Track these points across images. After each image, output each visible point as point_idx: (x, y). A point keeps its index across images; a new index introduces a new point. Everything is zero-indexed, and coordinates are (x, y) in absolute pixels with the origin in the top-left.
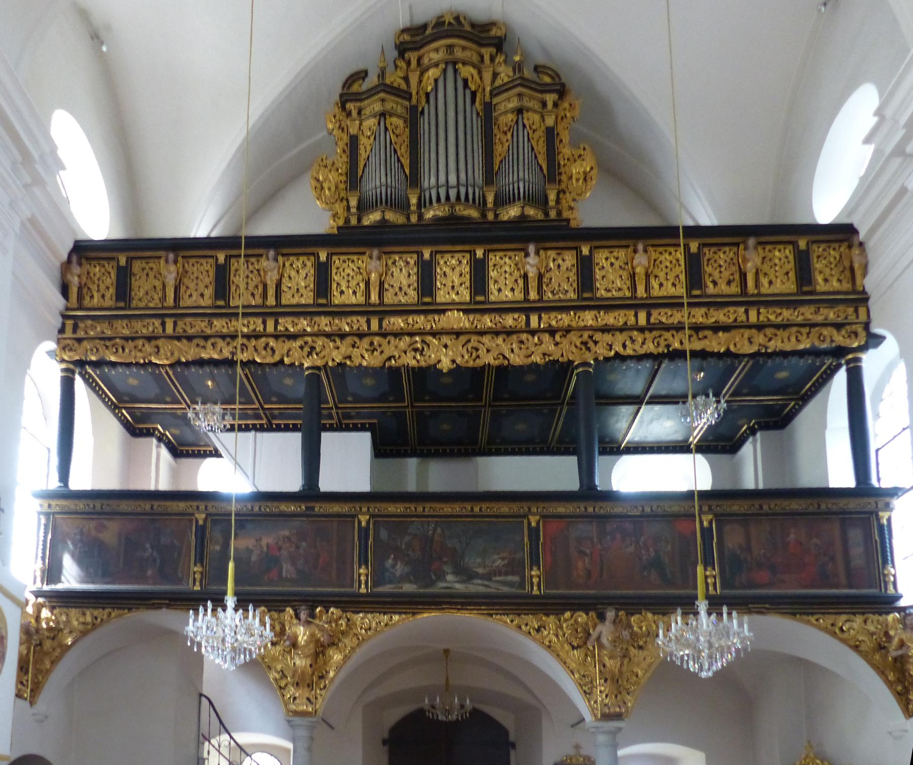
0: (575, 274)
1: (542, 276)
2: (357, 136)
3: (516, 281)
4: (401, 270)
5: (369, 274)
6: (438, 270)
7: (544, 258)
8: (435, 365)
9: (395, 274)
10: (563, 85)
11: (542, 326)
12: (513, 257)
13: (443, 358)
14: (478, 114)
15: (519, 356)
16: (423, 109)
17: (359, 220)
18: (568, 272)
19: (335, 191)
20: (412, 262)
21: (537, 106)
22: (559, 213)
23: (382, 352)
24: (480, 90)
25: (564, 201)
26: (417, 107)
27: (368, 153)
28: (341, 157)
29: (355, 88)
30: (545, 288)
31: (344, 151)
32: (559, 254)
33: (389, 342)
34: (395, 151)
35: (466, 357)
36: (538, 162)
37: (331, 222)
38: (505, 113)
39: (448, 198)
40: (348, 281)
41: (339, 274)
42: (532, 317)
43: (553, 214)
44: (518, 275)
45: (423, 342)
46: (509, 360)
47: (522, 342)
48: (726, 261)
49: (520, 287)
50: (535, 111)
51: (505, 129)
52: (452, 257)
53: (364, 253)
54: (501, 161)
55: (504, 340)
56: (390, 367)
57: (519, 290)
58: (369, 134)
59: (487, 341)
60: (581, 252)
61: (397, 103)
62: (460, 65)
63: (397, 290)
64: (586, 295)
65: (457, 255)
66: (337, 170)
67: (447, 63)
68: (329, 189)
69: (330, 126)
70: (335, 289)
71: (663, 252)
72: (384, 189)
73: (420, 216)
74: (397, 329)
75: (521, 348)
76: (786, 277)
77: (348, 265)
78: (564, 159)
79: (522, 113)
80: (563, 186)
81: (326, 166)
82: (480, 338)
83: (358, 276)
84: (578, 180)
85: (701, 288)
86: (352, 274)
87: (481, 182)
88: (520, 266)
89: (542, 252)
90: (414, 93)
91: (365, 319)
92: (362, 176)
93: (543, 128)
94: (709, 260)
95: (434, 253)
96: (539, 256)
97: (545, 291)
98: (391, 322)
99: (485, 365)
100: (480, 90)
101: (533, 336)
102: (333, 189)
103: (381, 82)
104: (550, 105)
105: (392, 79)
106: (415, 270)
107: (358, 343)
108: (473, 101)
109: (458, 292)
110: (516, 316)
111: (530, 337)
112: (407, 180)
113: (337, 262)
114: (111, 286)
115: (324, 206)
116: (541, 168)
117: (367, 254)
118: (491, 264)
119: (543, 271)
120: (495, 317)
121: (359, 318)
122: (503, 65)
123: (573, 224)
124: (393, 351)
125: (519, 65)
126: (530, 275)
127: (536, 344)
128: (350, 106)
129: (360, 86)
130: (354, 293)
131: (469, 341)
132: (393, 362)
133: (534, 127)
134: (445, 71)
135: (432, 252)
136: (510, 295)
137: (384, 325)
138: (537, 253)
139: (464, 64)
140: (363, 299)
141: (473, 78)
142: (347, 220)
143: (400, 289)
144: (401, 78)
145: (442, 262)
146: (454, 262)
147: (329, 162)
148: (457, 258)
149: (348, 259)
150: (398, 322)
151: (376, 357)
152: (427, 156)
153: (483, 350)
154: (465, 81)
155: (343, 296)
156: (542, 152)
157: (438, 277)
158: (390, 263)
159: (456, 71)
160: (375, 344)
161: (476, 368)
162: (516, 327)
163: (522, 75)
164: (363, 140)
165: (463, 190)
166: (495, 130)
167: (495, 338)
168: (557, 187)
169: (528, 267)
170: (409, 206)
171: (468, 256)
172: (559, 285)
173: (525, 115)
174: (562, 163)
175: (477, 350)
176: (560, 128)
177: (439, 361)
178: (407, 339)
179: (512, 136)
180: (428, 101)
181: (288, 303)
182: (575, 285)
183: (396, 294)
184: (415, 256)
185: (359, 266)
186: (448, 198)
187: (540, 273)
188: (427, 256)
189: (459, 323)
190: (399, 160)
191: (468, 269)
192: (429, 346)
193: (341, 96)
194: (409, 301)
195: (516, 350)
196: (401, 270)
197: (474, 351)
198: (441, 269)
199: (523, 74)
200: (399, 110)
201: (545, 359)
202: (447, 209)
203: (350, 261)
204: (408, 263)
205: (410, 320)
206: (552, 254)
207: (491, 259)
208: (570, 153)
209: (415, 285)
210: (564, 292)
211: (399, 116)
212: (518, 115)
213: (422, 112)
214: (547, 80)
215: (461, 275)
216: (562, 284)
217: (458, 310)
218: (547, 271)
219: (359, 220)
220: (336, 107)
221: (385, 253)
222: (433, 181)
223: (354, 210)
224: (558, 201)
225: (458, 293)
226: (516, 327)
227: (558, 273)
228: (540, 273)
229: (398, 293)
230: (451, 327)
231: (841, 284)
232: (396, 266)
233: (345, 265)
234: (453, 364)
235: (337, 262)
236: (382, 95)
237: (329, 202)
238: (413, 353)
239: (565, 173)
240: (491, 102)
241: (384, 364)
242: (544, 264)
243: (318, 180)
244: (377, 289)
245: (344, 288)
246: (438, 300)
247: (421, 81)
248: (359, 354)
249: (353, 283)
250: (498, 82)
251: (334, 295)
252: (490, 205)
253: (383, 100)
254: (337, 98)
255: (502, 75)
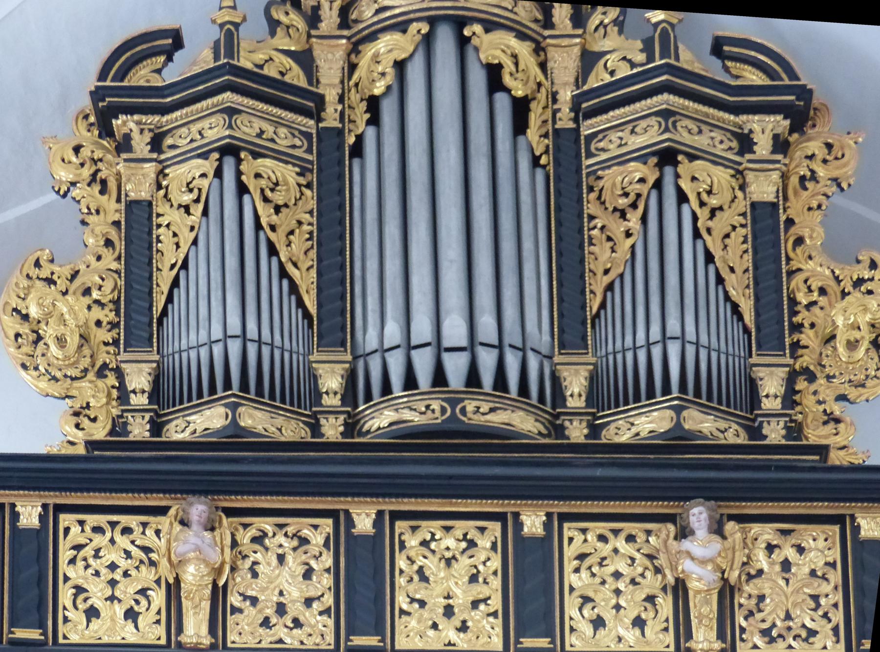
0: (836, 588)
1: (732, 589)
2: (150, 204)
4: (281, 558)
5: (177, 565)
6: (401, 563)
7: (739, 545)
10: (805, 93)
14: (535, 161)
16: (360, 138)
17: (157, 427)
18: (816, 582)
19: (81, 346)
20: (317, 539)
21: (723, 146)
22: (795, 430)
24: (542, 96)
25: (809, 401)
26: (340, 133)
27: (184, 249)
28: (99, 258)
29: (141, 76)
30: (740, 621)
31: (109, 243)
32: (785, 533)
34: (273, 251)
36: (726, 293)
37: (70, 429)
38: (621, 160)
39: (439, 378)
40: (113, 583)
41: (80, 564)
43: (774, 433)
49: (154, 608)
50: (717, 161)
51: (623, 202)
52: (448, 529)
53: (162, 511)
54: (610, 287)
57: (152, 616)
58: (187, 198)
60: (857, 529)
61: (278, 123)
62: (478, 28)
63: (269, 612)
65: (461, 526)
66: (87, 292)
67: (433, 21)
68: (61, 341)
69: (64, 175)
70: (69, 604)
72: (234, 347)
73: (352, 426)
76: (141, 529)
77: (112, 541)
78: (810, 290)
79: (676, 163)
80: (806, 360)
81: (50, 281)
83: (143, 568)
84: (852, 345)
86: (123, 564)
87: (546, 337)
90: (331, 95)
92: (164, 313)
93: (742, 205)
95: (387, 517)
96: (724, 538)
100: (542, 96)
102: (73, 341)
103: (223, 61)
104: (763, 146)
105: (260, 57)
108: (520, 125)
112: (311, 326)
113: (75, 529)
115: (43, 384)
116: (736, 309)
117: (172, 512)
118: (570, 552)
119: (733, 576)
122: (613, 30)
123: (836, 458)
125: (665, 35)
126: (693, 585)
128: (122, 123)
129: (159, 71)
130: (131, 615)
133: (714, 202)
134: (428, 40)
138: (717, 529)
139: (490, 26)
140: (161, 630)
141: (516, 64)
142: (118, 427)
144: (287, 53)
146: (450, 542)
147: (62, 272)
149: (113, 524)
152: (372, 265)
154: (494, 72)
155: (95, 624)
156: (739, 270)
157: (401, 581)
158: (245, 537)
159: (463, 42)
163: (672, 61)
164: (169, 215)
165: (487, 360)
166: (591, 207)
168: (788, 360)
169: (687, 565)
170: (317, 395)
172: (788, 617)
173: (685, 167)
174: (802, 298)
176: (796, 207)
179: (644, 219)
180: (374, 120)
182: (838, 617)
183: (266, 623)
186: (439, 378)
188: (364, 523)
190: (283, 273)
191: (496, 563)
193: (97, 95)
196: (281, 558)
198: (411, 560)
199: (677, 58)
200: (284, 140)
202: (436, 405)
203: (118, 529)
206: (766, 532)
208: (828, 272)
210: (804, 634)
211: (280, 156)
212: (660, 165)
213: (357, 150)
214: (754, 77)
215: (473, 579)
216: (795, 613)
218: (750, 577)
219: (157, 427)
220: (82, 126)
221: (230, 512)
222: (393, 332)
223: (139, 400)
224: (790, 398)
225: (463, 628)
227: (782, 583)
228: (725, 581)
229: (274, 620)
231: (379, 74)
232: (267, 549)
233: (100, 540)
235: (75, 529)
236: (228, 98)
237: (59, 375)
239: (813, 325)
240: (577, 130)
242: (740, 558)
243: (26, 317)
244: (206, 605)
245: (99, 604)
247: (353, 67)
249: (127, 590)
250: (598, 78)
251: (66, 620)
252: (575, 403)
253: (231, 112)
254: (86, 103)
255: (612, 60)
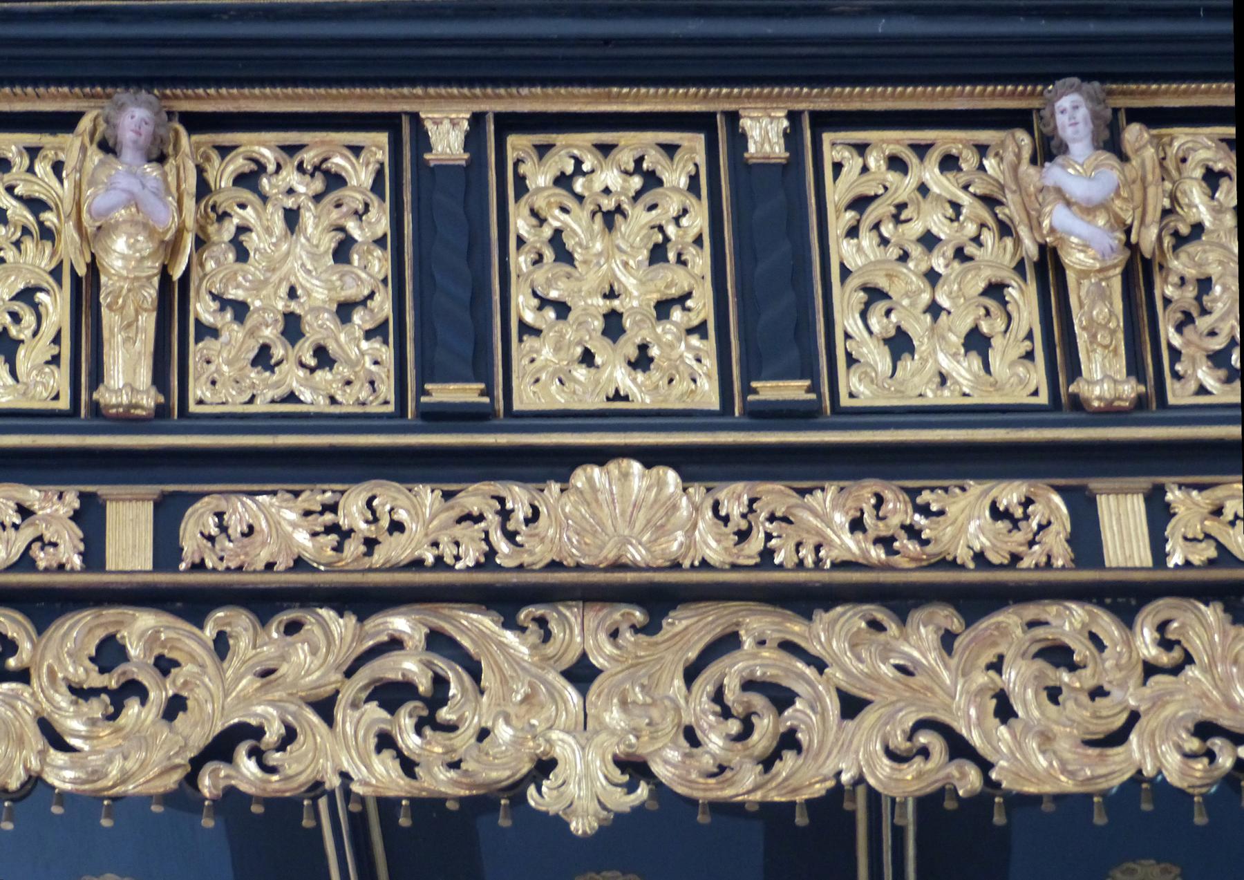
3: (995, 290)
4: (292, 218)
6: (521, 224)
8: (516, 790)
9: (252, 241)
11: (1176, 559)
12: (969, 161)
13: (564, 746)
15: (1046, 739)
20: (360, 175)
23: (175, 707)
30: (1169, 334)
33: (221, 646)
35: (715, 742)
42: (1107, 506)
44: (1008, 260)
45: (438, 641)
46: (985, 766)
47: (1058, 655)
48: (956, 207)
49: (48, 330)
52: (605, 149)
53: (65, 122)
55: (947, 640)
56: (232, 797)
59: (838, 645)
63: (270, 333)
64: (770, 390)
65: (631, 143)
71: (911, 158)
74: (270, 566)
75: (1054, 694)
82: (796, 629)
85: (807, 370)
88: (1011, 209)
89: (1134, 134)
91: (72, 501)
94: (860, 203)
95: (491, 128)
96: (1123, 158)
97: (1175, 354)
98: (236, 529)
99: (838, 792)
101: (1127, 618)
106: (380, 221)
107: (26, 646)
109: (643, 348)
110: (1010, 494)
111: (1108, 626)
114: (1014, 280)
117: (85, 124)
118: (838, 193)
119: (1148, 238)
120: (880, 501)
121: (32, 495)
124: (245, 700)
126: (1075, 259)
127: (1150, 669)
131: (727, 643)
132: (249, 767)
135: (477, 120)
136: (964, 371)
137: (190, 542)
143: (292, 327)
145: (540, 178)
146: (610, 177)
148: (628, 162)
150: (275, 524)
151: (142, 739)
153: (816, 703)
157: (520, 262)
158: (223, 174)
160: (134, 651)
161: (788, 808)
162: (1016, 558)
167: (893, 628)
169: (1058, 217)
171: (693, 144)
175: (781, 698)
177: (544, 767)
178: (341, 626)
181: (558, 399)
183: (263, 358)
184: (377, 143)
185: (38, 192)
187: (1132, 248)
189: (661, 530)
191: (698, 221)
192: (475, 671)
194: (348, 402)
195: (1027, 703)
196: (292, 218)
197: (758, 701)
198: (539, 218)
201: (1211, 755)
203: (934, 157)
204: (335, 181)
205: (352, 512)
207: (838, 167)
209: (383, 305)
215: (658, 254)
217: (650, 457)
218: (1180, 241)
221: (196, 123)
225: (642, 361)
226: (1016, 558)
228: (1132, 248)
229: (278, 352)
230: (610, 553)
234: (631, 788)
238: (374, 711)
241: (191, 779)
244: (148, 321)
246: (526, 397)
248: (28, 714)
